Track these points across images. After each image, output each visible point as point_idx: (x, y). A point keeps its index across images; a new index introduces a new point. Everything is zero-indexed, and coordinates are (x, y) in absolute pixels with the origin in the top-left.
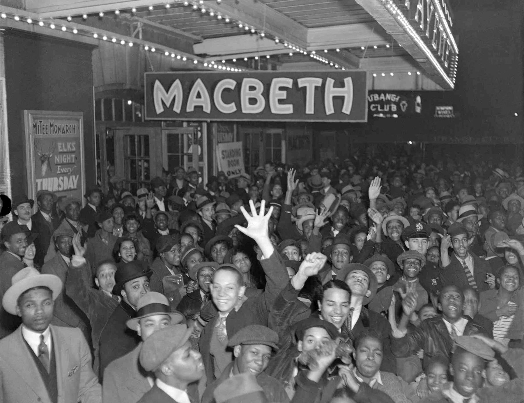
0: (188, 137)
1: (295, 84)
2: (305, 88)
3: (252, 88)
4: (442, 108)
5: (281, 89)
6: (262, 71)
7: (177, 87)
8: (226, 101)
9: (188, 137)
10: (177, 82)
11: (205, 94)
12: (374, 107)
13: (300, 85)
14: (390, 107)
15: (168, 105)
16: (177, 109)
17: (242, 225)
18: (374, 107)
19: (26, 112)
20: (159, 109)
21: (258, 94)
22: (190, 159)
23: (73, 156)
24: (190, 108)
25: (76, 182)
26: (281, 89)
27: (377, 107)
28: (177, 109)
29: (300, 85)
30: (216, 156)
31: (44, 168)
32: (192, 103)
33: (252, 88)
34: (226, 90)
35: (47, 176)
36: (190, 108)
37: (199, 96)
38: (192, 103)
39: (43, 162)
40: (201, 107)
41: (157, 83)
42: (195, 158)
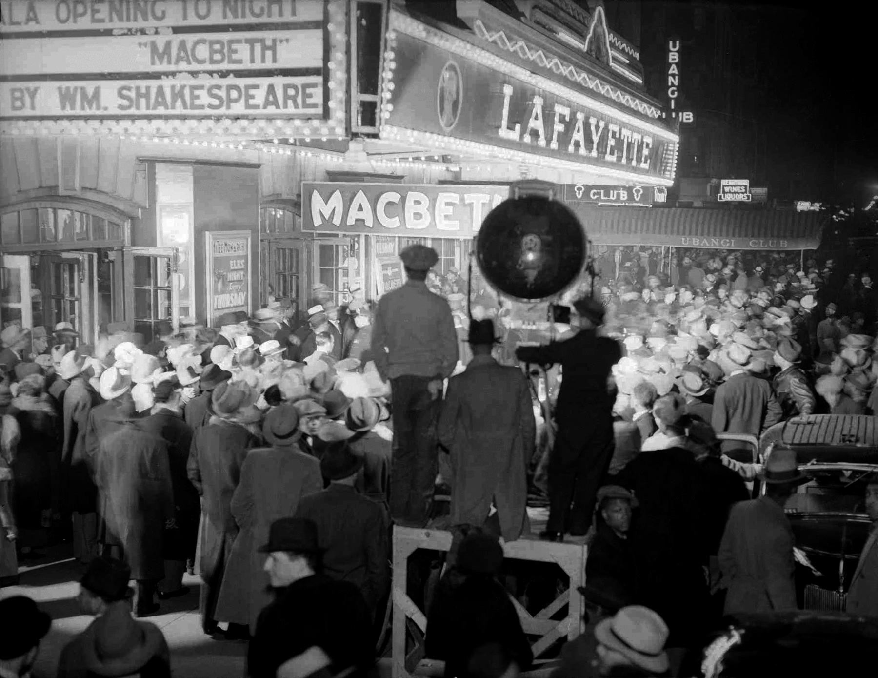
0: (344, 249)
1: (462, 199)
2: (471, 204)
3: (417, 202)
4: (732, 182)
5: (447, 204)
6: (428, 185)
7: (337, 200)
8: (389, 215)
9: (344, 249)
10: (337, 193)
11: (367, 206)
12: (594, 194)
13: (467, 202)
14: (618, 195)
15: (327, 217)
16: (337, 221)
17: (820, 496)
18: (594, 194)
19: (207, 233)
20: (317, 221)
21: (423, 208)
22: (346, 274)
23: (242, 273)
24: (351, 221)
25: (243, 298)
26: (447, 204)
27: (599, 194)
28: (337, 221)
29: (467, 202)
30: (348, 32)
31: (220, 285)
32: (353, 215)
33: (417, 202)
34: (390, 204)
35: (223, 292)
36: (351, 221)
37: (360, 208)
38: (353, 215)
39: (219, 279)
40: (363, 220)
41: (315, 193)
42: (352, 272)
